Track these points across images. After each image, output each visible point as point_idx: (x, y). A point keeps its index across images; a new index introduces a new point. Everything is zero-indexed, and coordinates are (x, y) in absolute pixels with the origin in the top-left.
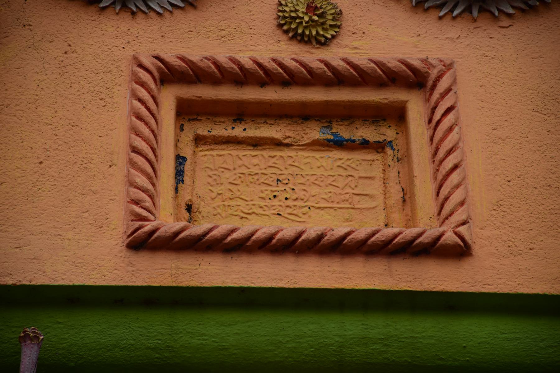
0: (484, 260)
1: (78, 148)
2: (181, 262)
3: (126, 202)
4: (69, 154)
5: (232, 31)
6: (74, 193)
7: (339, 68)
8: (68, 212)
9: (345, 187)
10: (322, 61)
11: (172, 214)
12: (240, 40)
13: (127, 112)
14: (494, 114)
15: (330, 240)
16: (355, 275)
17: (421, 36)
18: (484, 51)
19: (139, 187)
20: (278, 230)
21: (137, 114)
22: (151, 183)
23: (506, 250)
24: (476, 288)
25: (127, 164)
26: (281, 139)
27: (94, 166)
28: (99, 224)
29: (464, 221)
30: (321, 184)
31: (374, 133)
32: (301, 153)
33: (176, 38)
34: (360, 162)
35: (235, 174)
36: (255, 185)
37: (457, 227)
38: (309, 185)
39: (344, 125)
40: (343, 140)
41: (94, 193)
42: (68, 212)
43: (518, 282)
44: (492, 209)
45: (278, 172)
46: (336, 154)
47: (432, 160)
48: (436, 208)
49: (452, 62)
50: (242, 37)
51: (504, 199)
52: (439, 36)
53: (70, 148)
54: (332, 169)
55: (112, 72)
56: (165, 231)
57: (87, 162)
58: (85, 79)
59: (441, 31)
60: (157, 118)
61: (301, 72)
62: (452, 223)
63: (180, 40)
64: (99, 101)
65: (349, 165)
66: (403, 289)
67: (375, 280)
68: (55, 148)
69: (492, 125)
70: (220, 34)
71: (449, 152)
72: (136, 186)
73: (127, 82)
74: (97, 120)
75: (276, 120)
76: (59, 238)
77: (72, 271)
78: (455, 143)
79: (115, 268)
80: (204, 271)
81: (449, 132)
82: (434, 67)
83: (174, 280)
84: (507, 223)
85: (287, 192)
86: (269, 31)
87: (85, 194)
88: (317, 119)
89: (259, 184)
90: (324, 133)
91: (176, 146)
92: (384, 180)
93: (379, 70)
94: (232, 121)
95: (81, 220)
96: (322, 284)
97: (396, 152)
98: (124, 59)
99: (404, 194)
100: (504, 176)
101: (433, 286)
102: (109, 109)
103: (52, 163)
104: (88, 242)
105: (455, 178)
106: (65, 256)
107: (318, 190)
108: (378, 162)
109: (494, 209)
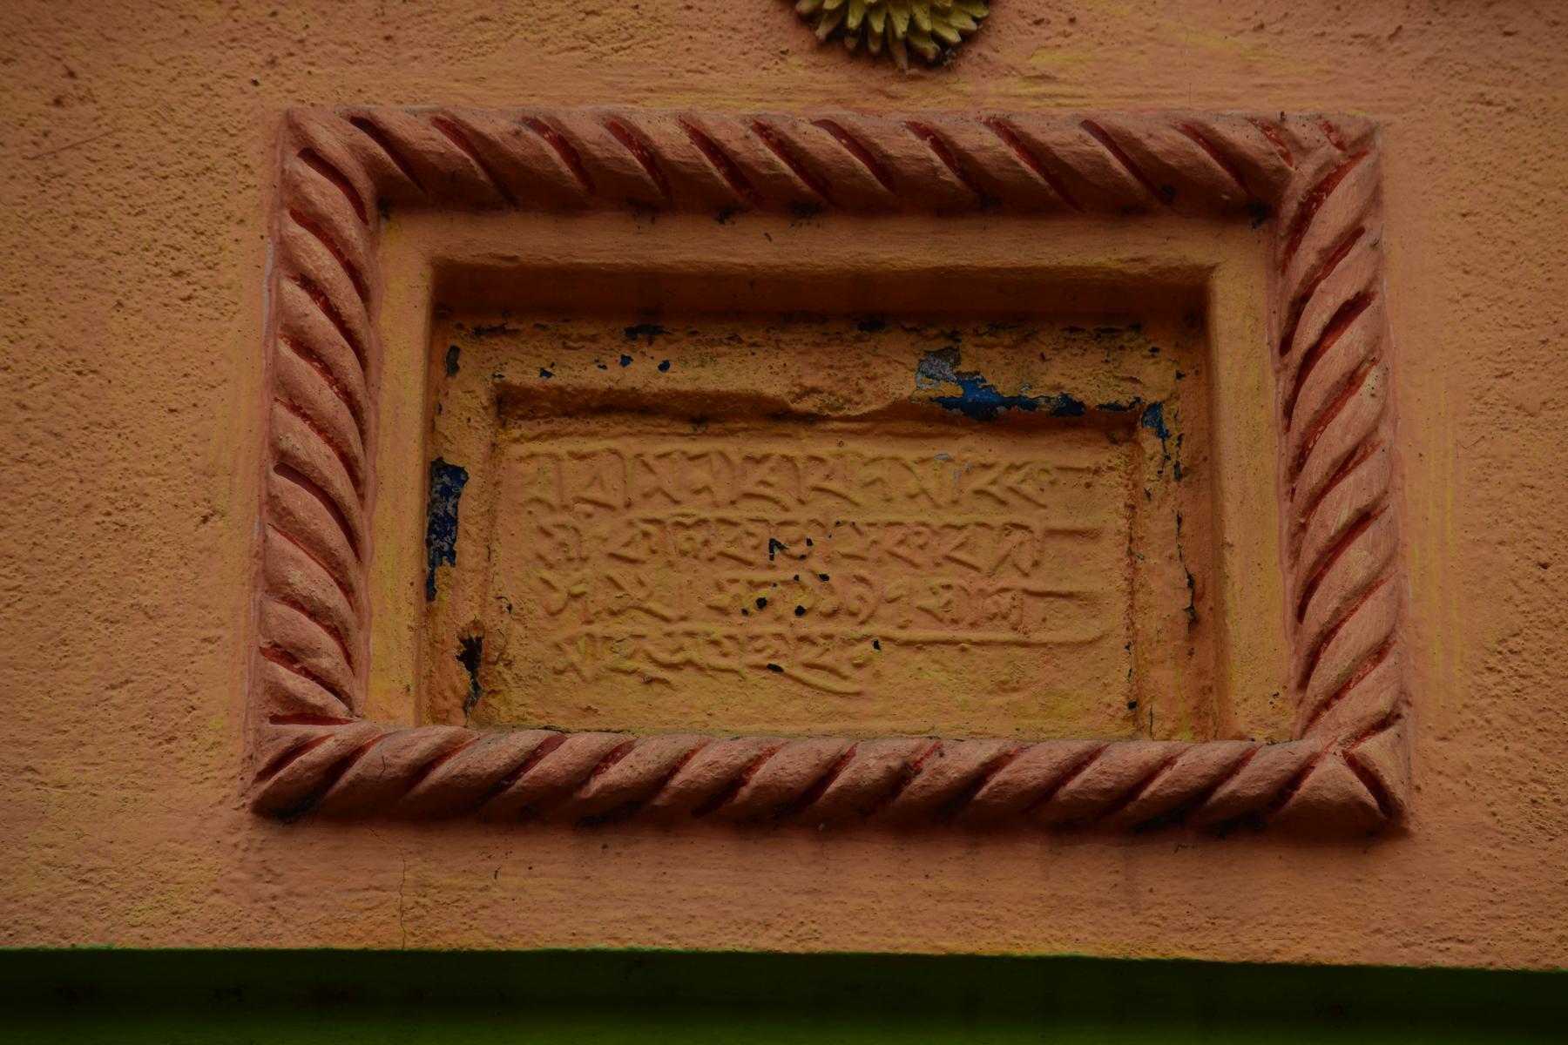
0: (1449, 852)
1: (96, 456)
2: (434, 864)
3: (255, 649)
4: (66, 475)
5: (622, 19)
6: (80, 617)
7: (983, 158)
8: (62, 687)
9: (997, 566)
10: (923, 131)
11: (409, 690)
12: (650, 51)
13: (265, 320)
14: (1506, 319)
15: (931, 789)
16: (1014, 908)
17: (1268, 28)
18: (1481, 82)
19: (300, 599)
20: (760, 753)
21: (295, 333)
22: (340, 584)
23: (1523, 813)
24: (1416, 952)
25: (261, 513)
26: (787, 399)
27: (151, 518)
28: (164, 729)
29: (1383, 717)
30: (919, 558)
31: (1101, 376)
32: (852, 446)
33: (434, 43)
34: (1052, 478)
35: (631, 524)
36: (696, 562)
37: (1356, 738)
38: (879, 561)
39: (1001, 344)
40: (996, 400)
41: (150, 618)
42: (62, 687)
43: (1559, 932)
44: (1481, 667)
45: (776, 515)
46: (971, 448)
47: (1288, 487)
48: (1295, 660)
49: (1366, 129)
50: (659, 38)
51: (1526, 631)
52: (1328, 29)
53: (68, 454)
54: (955, 502)
55: (214, 175)
56: (381, 761)
57: (127, 504)
58: (124, 197)
59: (1338, 8)
60: (366, 345)
61: (854, 173)
62: (1339, 725)
63: (446, 53)
64: (171, 280)
65: (1015, 486)
66: (1172, 957)
67: (1080, 923)
68: (20, 454)
69: (1495, 358)
70: (583, 27)
71: (1343, 467)
72: (288, 595)
73: (267, 209)
74: (163, 349)
75: (772, 332)
76: (29, 781)
77: (71, 898)
78: (1363, 434)
79: (214, 886)
80: (510, 895)
81: (1345, 392)
82: (1305, 151)
83: (409, 927)
84: (1530, 719)
85: (803, 588)
86: (749, 17)
87: (117, 622)
88: (908, 326)
89: (711, 560)
90: (931, 376)
91: (431, 428)
92: (1131, 540)
93: (1117, 164)
94: (623, 337)
95: (104, 715)
96: (904, 941)
97: (1171, 443)
98: (256, 124)
99: (1193, 598)
100: (1527, 545)
101: (1272, 946)
102: (203, 311)
103: (9, 510)
104: (124, 793)
105: (1357, 560)
106: (47, 846)
107: (907, 579)
108: (1111, 478)
109: (1491, 665)
